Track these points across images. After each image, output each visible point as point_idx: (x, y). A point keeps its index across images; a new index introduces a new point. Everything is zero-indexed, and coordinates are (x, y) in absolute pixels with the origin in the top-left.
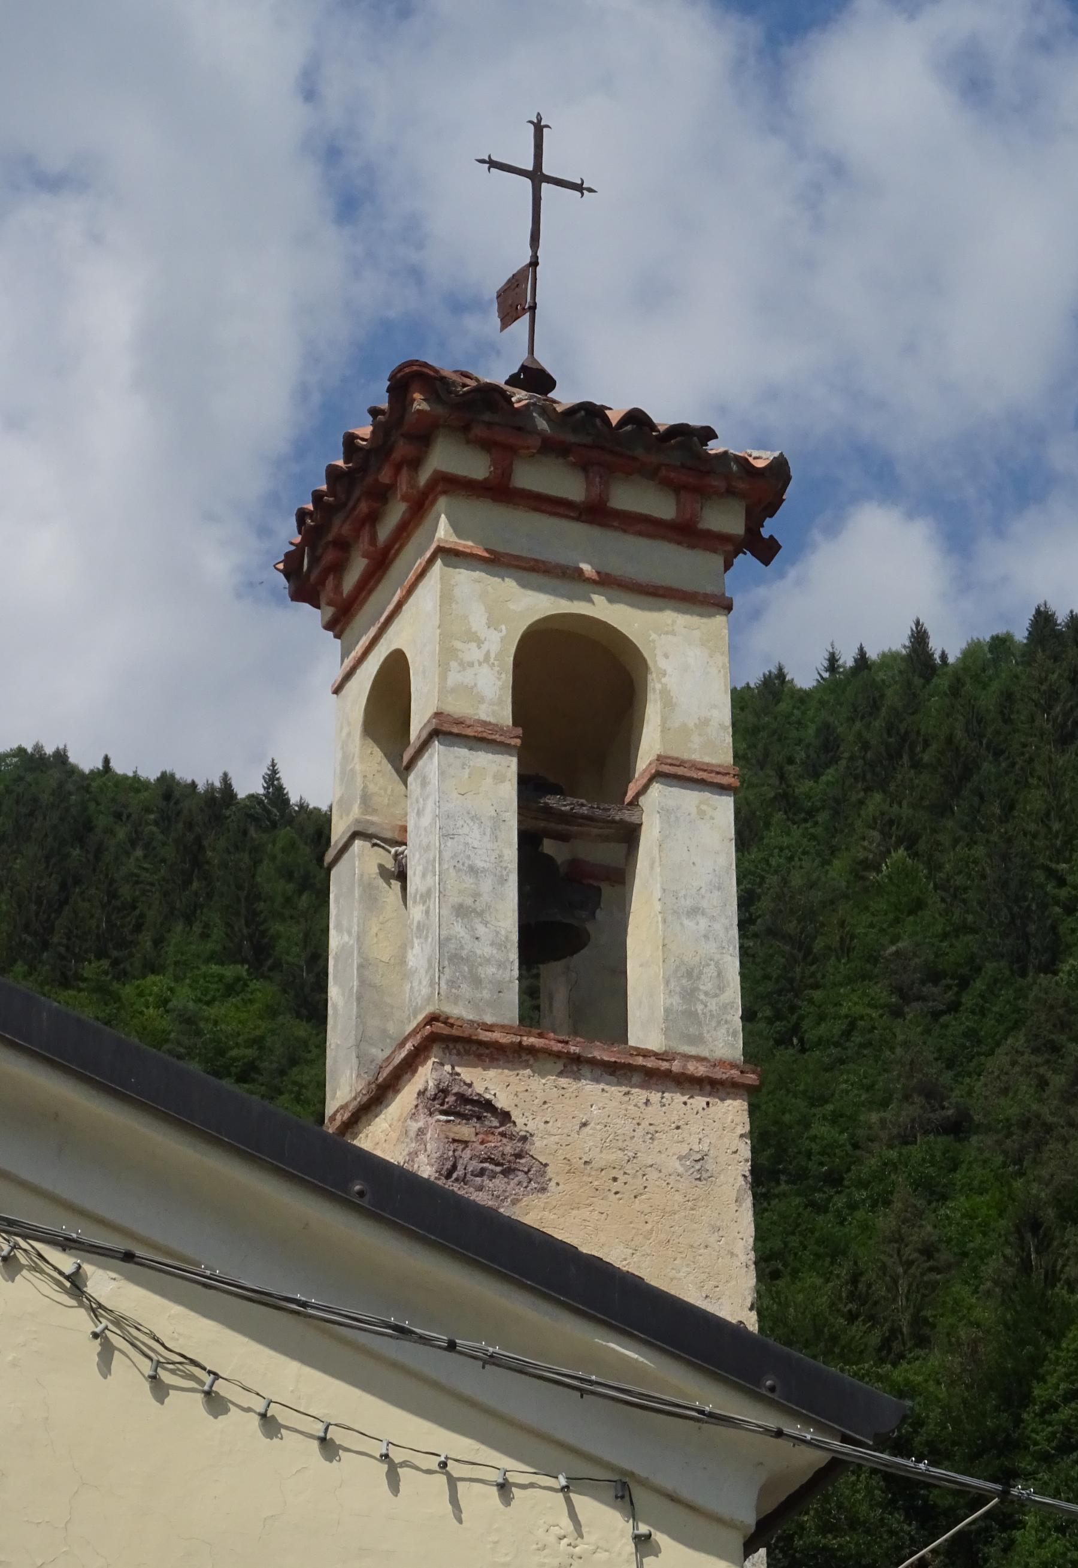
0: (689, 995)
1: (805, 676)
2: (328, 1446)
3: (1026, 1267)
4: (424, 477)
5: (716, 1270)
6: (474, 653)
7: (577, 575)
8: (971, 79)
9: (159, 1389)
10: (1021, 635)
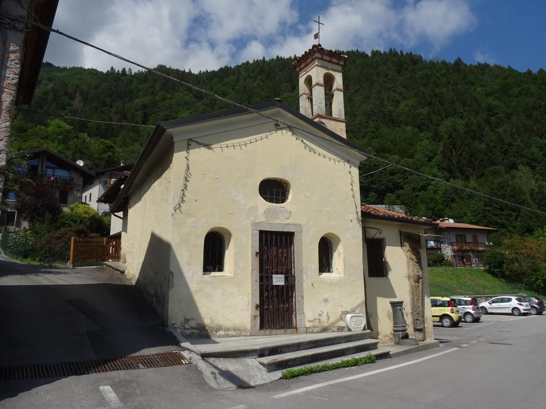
4: (314, 57)
9: (310, 151)
10: (275, 58)
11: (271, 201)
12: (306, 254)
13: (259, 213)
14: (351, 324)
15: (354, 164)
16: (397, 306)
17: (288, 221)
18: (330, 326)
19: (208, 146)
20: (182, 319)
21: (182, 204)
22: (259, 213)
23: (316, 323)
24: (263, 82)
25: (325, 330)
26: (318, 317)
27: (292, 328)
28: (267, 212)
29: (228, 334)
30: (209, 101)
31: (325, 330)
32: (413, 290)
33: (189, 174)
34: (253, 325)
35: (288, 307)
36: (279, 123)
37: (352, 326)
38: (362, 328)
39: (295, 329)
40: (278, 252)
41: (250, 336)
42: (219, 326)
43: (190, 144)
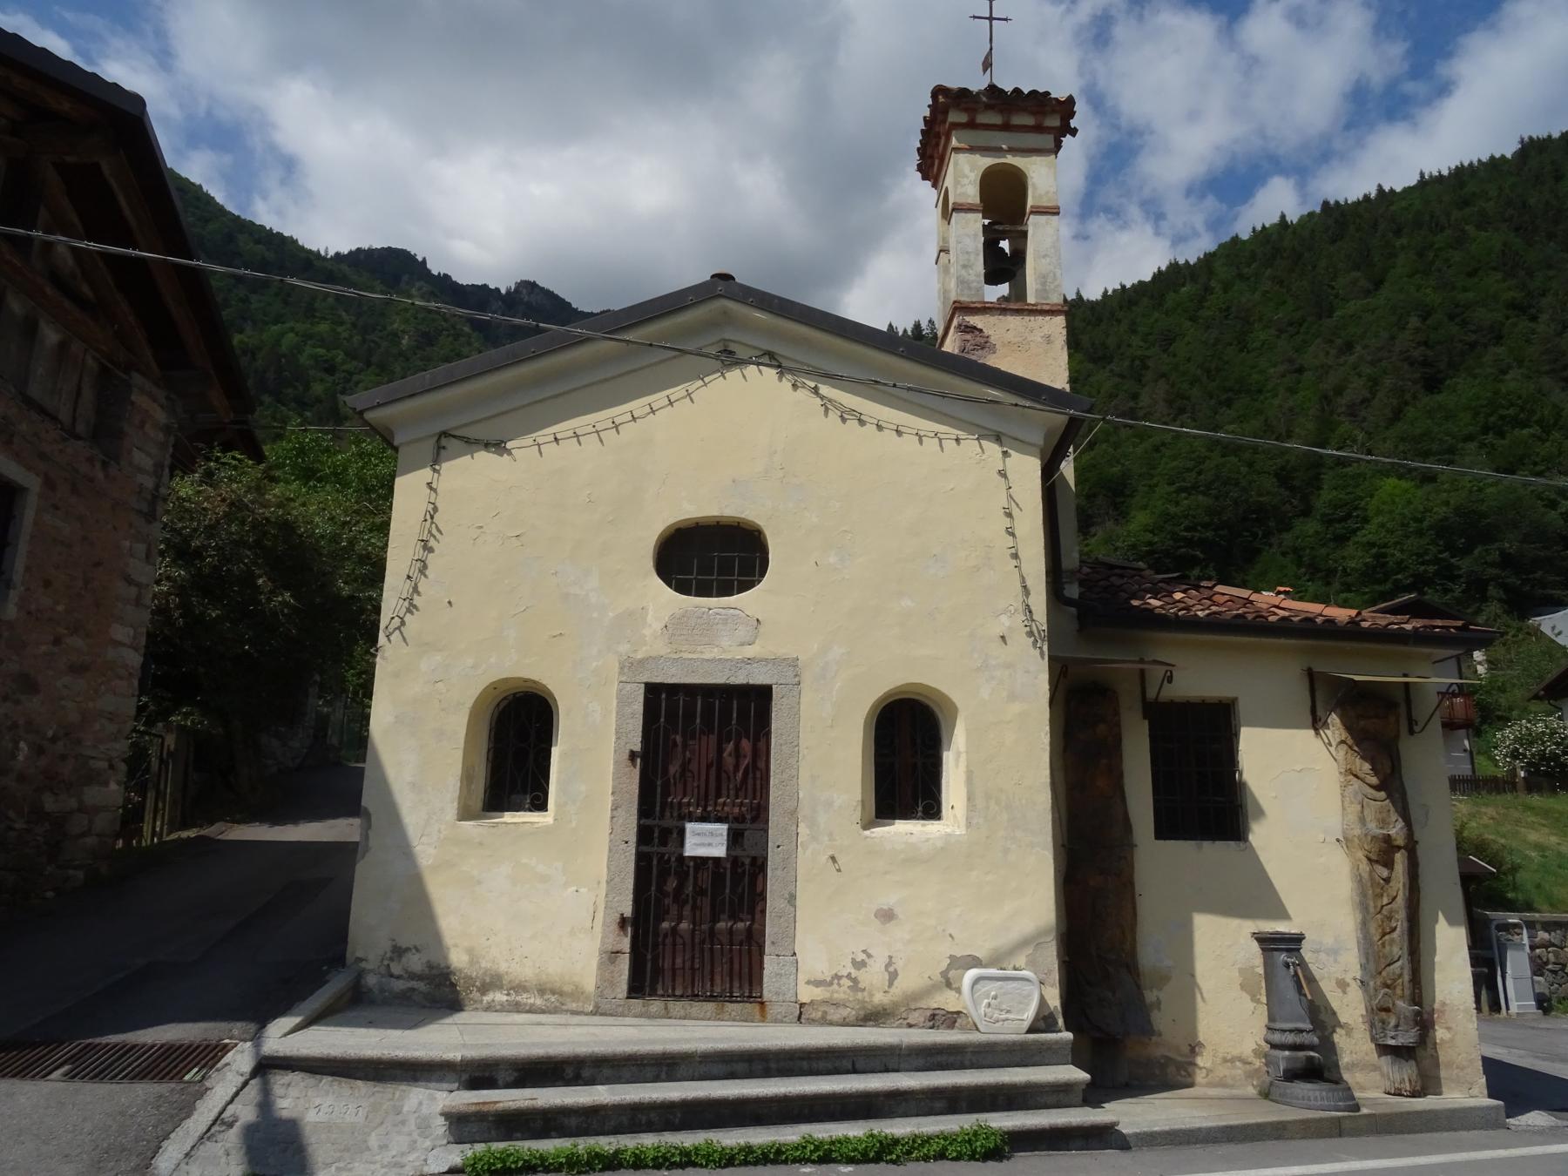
0: (1044, 284)
1: (1245, 236)
2: (899, 433)
3: (1323, 410)
5: (1054, 371)
6: (965, 181)
7: (1000, 150)
8: (1298, 18)
9: (844, 420)
11: (682, 588)
12: (820, 762)
13: (647, 632)
14: (976, 1004)
15: (1023, 446)
16: (1281, 948)
17: (750, 651)
18: (896, 1005)
19: (498, 446)
20: (385, 946)
21: (408, 618)
22: (647, 632)
23: (842, 992)
24: (1281, 283)
25: (873, 1017)
26: (850, 969)
27: (750, 998)
28: (675, 627)
29: (517, 1004)
30: (1127, 363)
31: (873, 1017)
32: (1363, 894)
33: (434, 531)
34: (605, 982)
35: (749, 930)
36: (732, 347)
37: (978, 1012)
38: (1026, 1025)
39: (757, 1007)
40: (720, 751)
41: (593, 1013)
42: (492, 976)
43: (444, 444)
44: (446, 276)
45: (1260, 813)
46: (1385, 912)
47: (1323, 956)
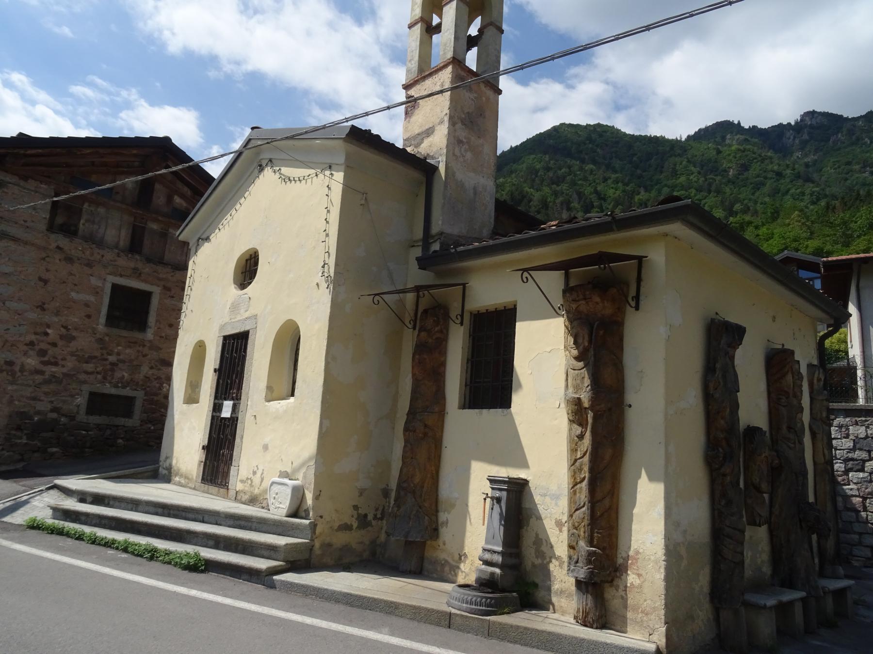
26: (251, 475)
44: (754, 127)
45: (520, 386)
46: (577, 464)
47: (548, 499)
